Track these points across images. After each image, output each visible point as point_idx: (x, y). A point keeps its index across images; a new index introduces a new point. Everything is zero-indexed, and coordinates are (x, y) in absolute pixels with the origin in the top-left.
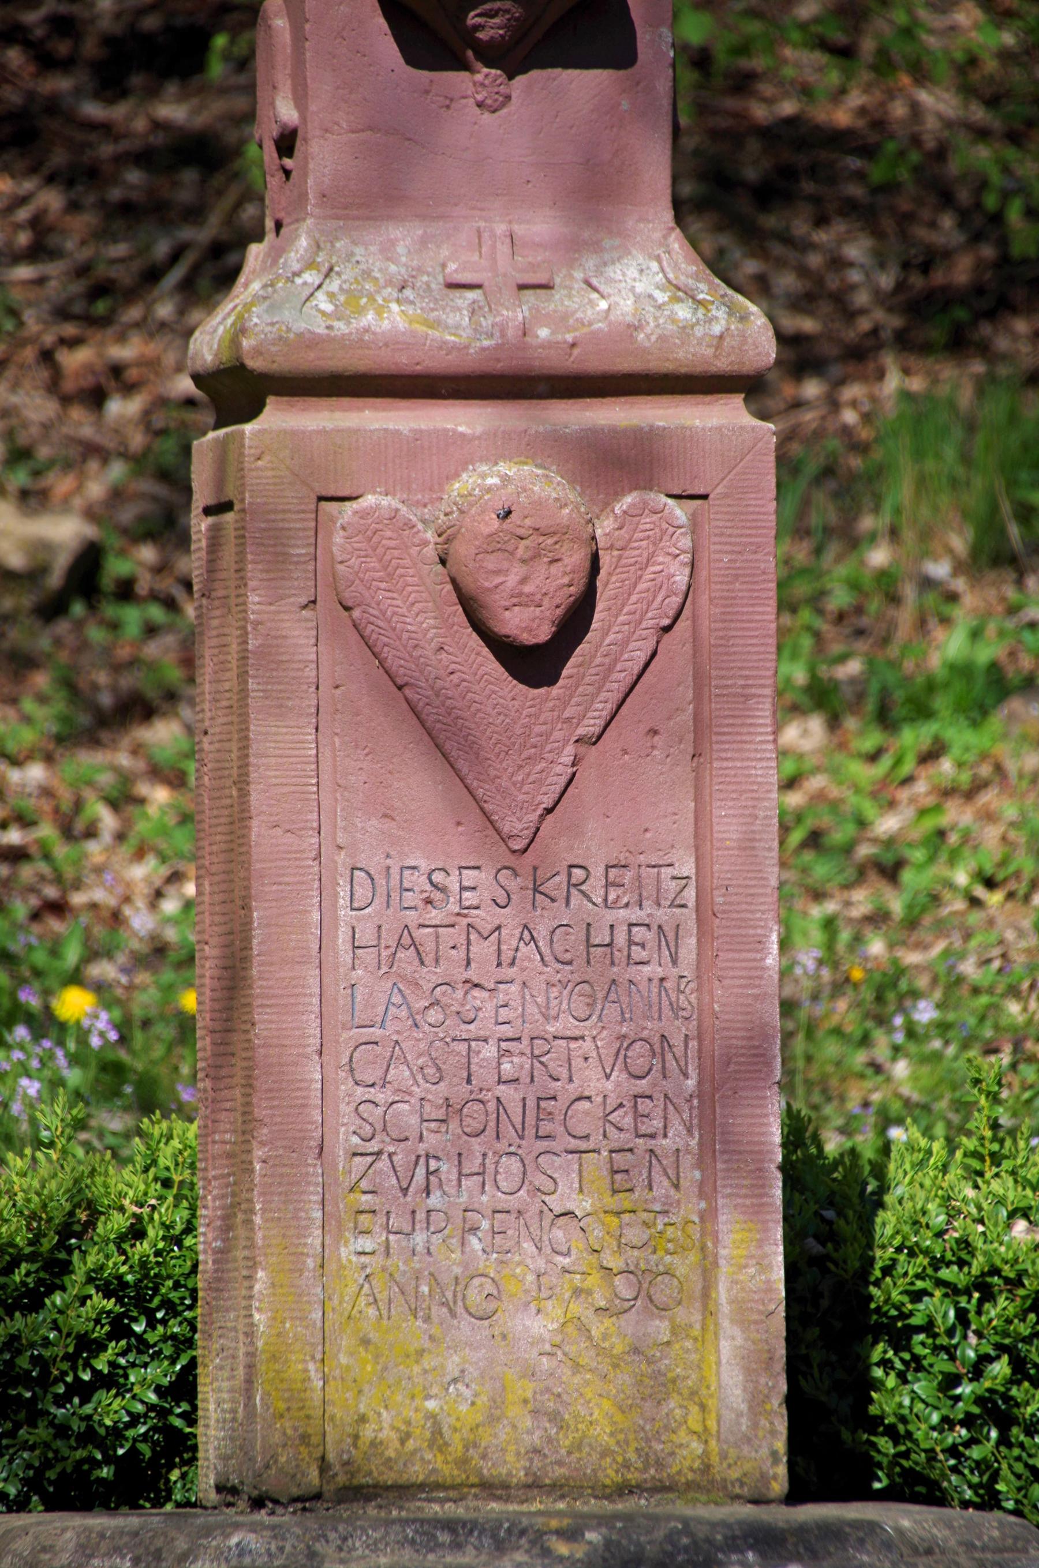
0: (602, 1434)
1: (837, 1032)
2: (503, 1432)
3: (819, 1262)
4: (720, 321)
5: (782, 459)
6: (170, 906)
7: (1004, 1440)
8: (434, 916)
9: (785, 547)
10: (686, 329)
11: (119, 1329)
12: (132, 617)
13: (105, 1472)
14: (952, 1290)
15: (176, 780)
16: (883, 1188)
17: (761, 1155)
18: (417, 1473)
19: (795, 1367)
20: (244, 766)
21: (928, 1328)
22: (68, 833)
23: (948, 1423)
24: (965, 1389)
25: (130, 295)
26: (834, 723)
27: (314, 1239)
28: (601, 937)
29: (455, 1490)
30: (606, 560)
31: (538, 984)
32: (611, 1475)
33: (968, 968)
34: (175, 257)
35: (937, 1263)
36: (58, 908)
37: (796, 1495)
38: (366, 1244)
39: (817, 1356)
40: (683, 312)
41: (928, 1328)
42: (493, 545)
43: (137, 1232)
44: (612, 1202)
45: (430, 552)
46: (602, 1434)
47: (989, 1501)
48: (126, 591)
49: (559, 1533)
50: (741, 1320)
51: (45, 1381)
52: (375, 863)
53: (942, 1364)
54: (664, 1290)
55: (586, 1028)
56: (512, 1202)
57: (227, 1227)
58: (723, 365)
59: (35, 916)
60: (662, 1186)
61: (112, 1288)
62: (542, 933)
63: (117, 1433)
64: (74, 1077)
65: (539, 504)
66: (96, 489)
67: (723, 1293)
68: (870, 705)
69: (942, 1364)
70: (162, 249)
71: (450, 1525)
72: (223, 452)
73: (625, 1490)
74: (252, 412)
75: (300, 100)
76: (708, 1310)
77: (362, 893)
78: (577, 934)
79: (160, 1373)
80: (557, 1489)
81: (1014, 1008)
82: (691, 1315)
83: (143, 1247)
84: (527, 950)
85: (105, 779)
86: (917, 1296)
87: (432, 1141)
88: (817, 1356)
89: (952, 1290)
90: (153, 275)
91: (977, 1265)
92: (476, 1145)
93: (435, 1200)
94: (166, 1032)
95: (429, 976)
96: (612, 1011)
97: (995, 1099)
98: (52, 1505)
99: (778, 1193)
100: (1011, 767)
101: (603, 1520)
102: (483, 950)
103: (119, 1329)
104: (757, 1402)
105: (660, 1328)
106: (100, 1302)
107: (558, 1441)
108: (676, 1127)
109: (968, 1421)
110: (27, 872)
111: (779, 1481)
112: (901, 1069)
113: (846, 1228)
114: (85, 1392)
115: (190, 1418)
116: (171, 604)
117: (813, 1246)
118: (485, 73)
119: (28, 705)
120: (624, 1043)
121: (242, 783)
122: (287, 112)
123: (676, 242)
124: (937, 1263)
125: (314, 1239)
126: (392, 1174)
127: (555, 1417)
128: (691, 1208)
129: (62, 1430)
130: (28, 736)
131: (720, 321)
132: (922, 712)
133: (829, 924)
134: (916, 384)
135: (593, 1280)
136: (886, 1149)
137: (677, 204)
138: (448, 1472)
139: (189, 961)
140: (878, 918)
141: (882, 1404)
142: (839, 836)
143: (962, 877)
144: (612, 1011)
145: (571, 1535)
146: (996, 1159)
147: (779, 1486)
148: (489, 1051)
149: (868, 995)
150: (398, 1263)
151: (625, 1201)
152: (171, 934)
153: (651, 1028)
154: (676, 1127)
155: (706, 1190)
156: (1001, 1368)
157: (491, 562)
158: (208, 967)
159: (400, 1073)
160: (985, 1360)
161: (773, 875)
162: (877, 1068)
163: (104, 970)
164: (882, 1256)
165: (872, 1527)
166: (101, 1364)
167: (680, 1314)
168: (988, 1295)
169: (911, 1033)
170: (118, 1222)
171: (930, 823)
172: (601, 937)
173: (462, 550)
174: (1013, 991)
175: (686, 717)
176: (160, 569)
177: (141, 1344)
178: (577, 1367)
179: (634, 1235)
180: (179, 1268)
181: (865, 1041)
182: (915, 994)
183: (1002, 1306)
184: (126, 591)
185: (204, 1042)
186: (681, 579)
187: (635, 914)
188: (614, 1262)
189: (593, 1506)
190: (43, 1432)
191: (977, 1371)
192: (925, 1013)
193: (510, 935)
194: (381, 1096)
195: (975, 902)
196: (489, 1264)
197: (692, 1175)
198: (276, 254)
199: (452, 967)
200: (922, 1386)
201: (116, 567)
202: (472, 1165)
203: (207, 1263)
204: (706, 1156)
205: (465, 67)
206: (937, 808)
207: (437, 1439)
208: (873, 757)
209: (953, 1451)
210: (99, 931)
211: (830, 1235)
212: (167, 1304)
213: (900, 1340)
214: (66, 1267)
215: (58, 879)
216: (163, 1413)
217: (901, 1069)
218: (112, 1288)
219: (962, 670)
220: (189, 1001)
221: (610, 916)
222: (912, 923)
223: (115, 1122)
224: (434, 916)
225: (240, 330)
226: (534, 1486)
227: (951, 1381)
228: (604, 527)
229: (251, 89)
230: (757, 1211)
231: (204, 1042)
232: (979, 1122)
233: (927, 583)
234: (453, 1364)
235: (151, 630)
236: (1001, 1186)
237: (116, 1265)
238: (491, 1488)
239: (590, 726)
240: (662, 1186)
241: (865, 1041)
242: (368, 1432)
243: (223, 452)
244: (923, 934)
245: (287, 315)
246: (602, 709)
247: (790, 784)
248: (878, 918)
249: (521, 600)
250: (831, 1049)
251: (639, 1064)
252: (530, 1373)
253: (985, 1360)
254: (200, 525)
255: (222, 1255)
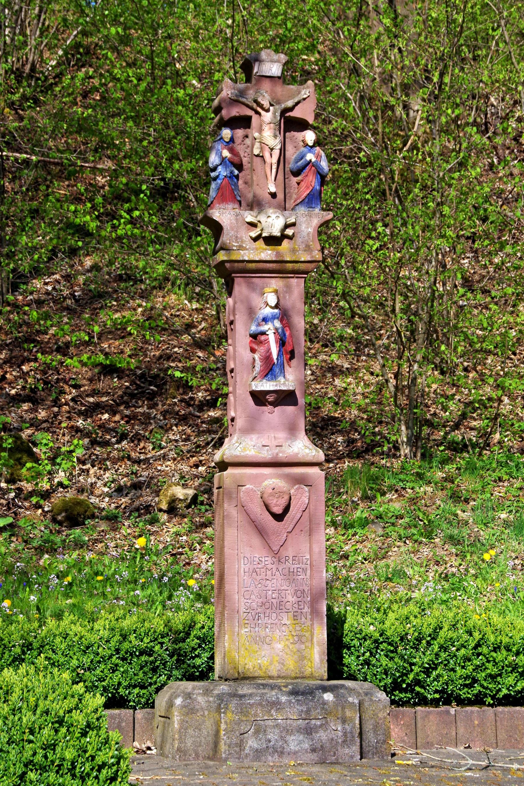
0: (292, 667)
1: (337, 588)
2: (273, 667)
3: (333, 633)
4: (314, 453)
5: (326, 478)
6: (210, 564)
7: (368, 668)
8: (260, 566)
9: (327, 495)
10: (307, 454)
11: (200, 646)
12: (203, 508)
13: (197, 674)
14: (359, 639)
15: (211, 539)
16: (346, 619)
17: (322, 613)
18: (256, 674)
19: (329, 654)
20: (223, 537)
21: (354, 646)
22: (191, 550)
23: (358, 665)
24: (361, 658)
25: (204, 447)
26: (336, 529)
27: (237, 629)
28: (292, 570)
29: (263, 678)
30: (292, 498)
31: (280, 579)
32: (293, 675)
33: (361, 576)
34: (212, 440)
35: (356, 634)
36: (189, 564)
37: (329, 679)
38: (247, 630)
39: (333, 652)
40: (307, 451)
41: (354, 646)
42: (271, 495)
43: (203, 627)
44: (294, 622)
45: (259, 496)
46: (292, 667)
47: (365, 680)
48: (202, 503)
49: (284, 686)
50: (319, 646)
51: (186, 656)
52: (248, 556)
53: (357, 653)
54: (304, 639)
55: (289, 588)
56: (274, 622)
57: (220, 627)
58: (315, 461)
59: (184, 565)
60: (303, 619)
61: (198, 638)
62: (280, 569)
63: (199, 666)
64: (191, 597)
65: (280, 487)
66: (196, 484)
67: (315, 640)
68: (343, 525)
69: (357, 653)
70: (209, 439)
71: (263, 685)
72: (220, 478)
73: (296, 678)
74: (225, 469)
75: (235, 411)
76: (312, 644)
77: (246, 562)
78: (287, 570)
79: (207, 655)
80: (283, 678)
81: (370, 583)
82: (308, 644)
83: (204, 630)
84: (278, 573)
85: (198, 539)
86: (352, 640)
87: (259, 610)
88: (333, 652)
89: (359, 639)
90: (208, 444)
91: (363, 634)
92: (268, 611)
93: (260, 622)
94: (209, 588)
95: (258, 578)
96: (294, 585)
97: (367, 602)
98: (188, 680)
99: (325, 620)
100: (369, 537)
101: (292, 684)
102: (269, 573)
103: (200, 646)
104: (321, 661)
105: (303, 647)
106: (196, 641)
107: (389, 38)
108: (306, 608)
109: (362, 664)
110: (183, 557)
111: (326, 676)
112: (349, 595)
113: (339, 627)
114: (193, 658)
115: (213, 663)
116: (210, 506)
117: (332, 630)
118: (270, 407)
119: (183, 525)
120: (296, 591)
121: (223, 540)
122: (232, 414)
123: (306, 438)
124: (356, 634)
125: (237, 629)
126: (294, 259)
127: (283, 664)
128: (309, 623)
129: (189, 665)
130: (183, 531)
131: (314, 453)
132: (352, 526)
133: (335, 567)
134: (351, 464)
135: (290, 637)
136: (346, 611)
137: (306, 430)
138: (262, 674)
139: (213, 574)
140: (344, 566)
141: (345, 661)
142: (337, 550)
143: (360, 558)
144: (294, 585)
145: (286, 686)
146: (367, 614)
147: (326, 677)
148: (270, 593)
149: (342, 581)
150: (253, 634)
151: (296, 622)
152: (210, 569)
153: (301, 588)
154: (306, 608)
155: (312, 620)
156: (368, 654)
157: (271, 498)
158: (216, 576)
159: (253, 597)
160: (365, 652)
161: (325, 558)
162: (344, 595)
163: (197, 576)
164: (345, 632)
165: (343, 686)
166: (196, 653)
167: (307, 644)
168: (365, 640)
169: (351, 588)
170: (199, 625)
171: (354, 548)
172: (292, 570)
173: (265, 496)
174: (370, 580)
175: (308, 528)
176: (208, 499)
177: (204, 649)
178: (287, 654)
179: (298, 628)
180: (211, 634)
181: (342, 590)
182: (351, 581)
183: (368, 642)
184: (202, 503)
185: (216, 591)
186: (307, 501)
187: (298, 566)
188: (294, 634)
189: (290, 681)
190: (185, 666)
191: (363, 655)
192: (353, 585)
193: (274, 570)
194: (249, 601)
195: (363, 563)
196: (270, 634)
197: (309, 617)
198: (230, 440)
199: (263, 576)
200: (353, 658)
201: (201, 498)
202: (267, 615)
203: (216, 633)
204: (312, 613)
205: (266, 405)
206: (356, 545)
207: (260, 668)
208: (343, 535)
209: (359, 670)
210: (196, 568)
211: (335, 628)
212: (209, 641)
213: (349, 649)
214: (190, 634)
215: (189, 559)
216: (208, 662)
217: (349, 595)
218: (198, 638)
219: (360, 519)
220: (213, 582)
221: (293, 566)
222: (351, 567)
223: (199, 605)
224: (260, 566)
225: (223, 454)
226: (279, 677)
227: (358, 657)
228: (292, 491)
229: (226, 410)
230: (322, 624)
231: (216, 591)
232: (363, 606)
233: (353, 502)
234: (263, 653)
235: (207, 510)
236: (368, 619)
237: (199, 634)
238: (271, 677)
239: (289, 530)
240: (303, 619)
241: (342, 590)
242: (247, 667)
243: (220, 478)
244: (353, 569)
245: (232, 451)
246: (292, 526)
247: (328, 540)
248: (344, 566)
249: (276, 505)
250: (336, 591)
251: (299, 595)
252: (278, 655)
253: (365, 652)
254: (215, 491)
255: (219, 632)
